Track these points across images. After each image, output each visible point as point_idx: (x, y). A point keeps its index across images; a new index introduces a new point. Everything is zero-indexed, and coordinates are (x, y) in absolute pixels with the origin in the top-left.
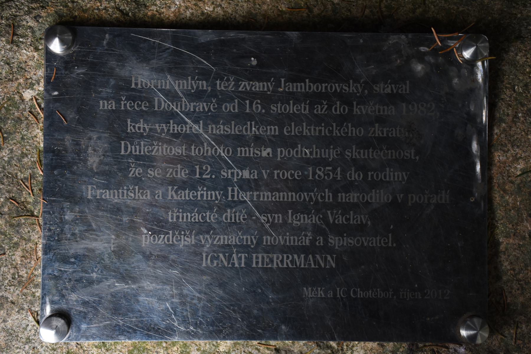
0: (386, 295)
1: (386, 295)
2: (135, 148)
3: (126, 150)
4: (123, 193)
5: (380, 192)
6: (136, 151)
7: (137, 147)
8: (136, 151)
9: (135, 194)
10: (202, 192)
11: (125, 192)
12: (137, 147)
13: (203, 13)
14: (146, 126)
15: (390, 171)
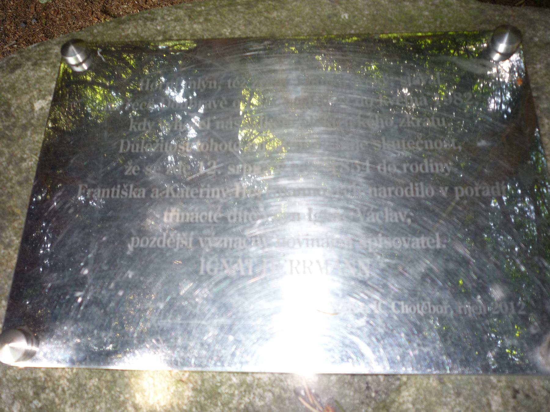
0: (469, 192)
1: (469, 192)
2: (135, 146)
3: (125, 147)
4: (116, 191)
5: (419, 186)
6: (135, 149)
7: (138, 145)
8: (135, 149)
9: (128, 193)
10: (205, 189)
11: (118, 191)
12: (138, 145)
13: (220, 34)
14: (149, 124)
15: (429, 163)
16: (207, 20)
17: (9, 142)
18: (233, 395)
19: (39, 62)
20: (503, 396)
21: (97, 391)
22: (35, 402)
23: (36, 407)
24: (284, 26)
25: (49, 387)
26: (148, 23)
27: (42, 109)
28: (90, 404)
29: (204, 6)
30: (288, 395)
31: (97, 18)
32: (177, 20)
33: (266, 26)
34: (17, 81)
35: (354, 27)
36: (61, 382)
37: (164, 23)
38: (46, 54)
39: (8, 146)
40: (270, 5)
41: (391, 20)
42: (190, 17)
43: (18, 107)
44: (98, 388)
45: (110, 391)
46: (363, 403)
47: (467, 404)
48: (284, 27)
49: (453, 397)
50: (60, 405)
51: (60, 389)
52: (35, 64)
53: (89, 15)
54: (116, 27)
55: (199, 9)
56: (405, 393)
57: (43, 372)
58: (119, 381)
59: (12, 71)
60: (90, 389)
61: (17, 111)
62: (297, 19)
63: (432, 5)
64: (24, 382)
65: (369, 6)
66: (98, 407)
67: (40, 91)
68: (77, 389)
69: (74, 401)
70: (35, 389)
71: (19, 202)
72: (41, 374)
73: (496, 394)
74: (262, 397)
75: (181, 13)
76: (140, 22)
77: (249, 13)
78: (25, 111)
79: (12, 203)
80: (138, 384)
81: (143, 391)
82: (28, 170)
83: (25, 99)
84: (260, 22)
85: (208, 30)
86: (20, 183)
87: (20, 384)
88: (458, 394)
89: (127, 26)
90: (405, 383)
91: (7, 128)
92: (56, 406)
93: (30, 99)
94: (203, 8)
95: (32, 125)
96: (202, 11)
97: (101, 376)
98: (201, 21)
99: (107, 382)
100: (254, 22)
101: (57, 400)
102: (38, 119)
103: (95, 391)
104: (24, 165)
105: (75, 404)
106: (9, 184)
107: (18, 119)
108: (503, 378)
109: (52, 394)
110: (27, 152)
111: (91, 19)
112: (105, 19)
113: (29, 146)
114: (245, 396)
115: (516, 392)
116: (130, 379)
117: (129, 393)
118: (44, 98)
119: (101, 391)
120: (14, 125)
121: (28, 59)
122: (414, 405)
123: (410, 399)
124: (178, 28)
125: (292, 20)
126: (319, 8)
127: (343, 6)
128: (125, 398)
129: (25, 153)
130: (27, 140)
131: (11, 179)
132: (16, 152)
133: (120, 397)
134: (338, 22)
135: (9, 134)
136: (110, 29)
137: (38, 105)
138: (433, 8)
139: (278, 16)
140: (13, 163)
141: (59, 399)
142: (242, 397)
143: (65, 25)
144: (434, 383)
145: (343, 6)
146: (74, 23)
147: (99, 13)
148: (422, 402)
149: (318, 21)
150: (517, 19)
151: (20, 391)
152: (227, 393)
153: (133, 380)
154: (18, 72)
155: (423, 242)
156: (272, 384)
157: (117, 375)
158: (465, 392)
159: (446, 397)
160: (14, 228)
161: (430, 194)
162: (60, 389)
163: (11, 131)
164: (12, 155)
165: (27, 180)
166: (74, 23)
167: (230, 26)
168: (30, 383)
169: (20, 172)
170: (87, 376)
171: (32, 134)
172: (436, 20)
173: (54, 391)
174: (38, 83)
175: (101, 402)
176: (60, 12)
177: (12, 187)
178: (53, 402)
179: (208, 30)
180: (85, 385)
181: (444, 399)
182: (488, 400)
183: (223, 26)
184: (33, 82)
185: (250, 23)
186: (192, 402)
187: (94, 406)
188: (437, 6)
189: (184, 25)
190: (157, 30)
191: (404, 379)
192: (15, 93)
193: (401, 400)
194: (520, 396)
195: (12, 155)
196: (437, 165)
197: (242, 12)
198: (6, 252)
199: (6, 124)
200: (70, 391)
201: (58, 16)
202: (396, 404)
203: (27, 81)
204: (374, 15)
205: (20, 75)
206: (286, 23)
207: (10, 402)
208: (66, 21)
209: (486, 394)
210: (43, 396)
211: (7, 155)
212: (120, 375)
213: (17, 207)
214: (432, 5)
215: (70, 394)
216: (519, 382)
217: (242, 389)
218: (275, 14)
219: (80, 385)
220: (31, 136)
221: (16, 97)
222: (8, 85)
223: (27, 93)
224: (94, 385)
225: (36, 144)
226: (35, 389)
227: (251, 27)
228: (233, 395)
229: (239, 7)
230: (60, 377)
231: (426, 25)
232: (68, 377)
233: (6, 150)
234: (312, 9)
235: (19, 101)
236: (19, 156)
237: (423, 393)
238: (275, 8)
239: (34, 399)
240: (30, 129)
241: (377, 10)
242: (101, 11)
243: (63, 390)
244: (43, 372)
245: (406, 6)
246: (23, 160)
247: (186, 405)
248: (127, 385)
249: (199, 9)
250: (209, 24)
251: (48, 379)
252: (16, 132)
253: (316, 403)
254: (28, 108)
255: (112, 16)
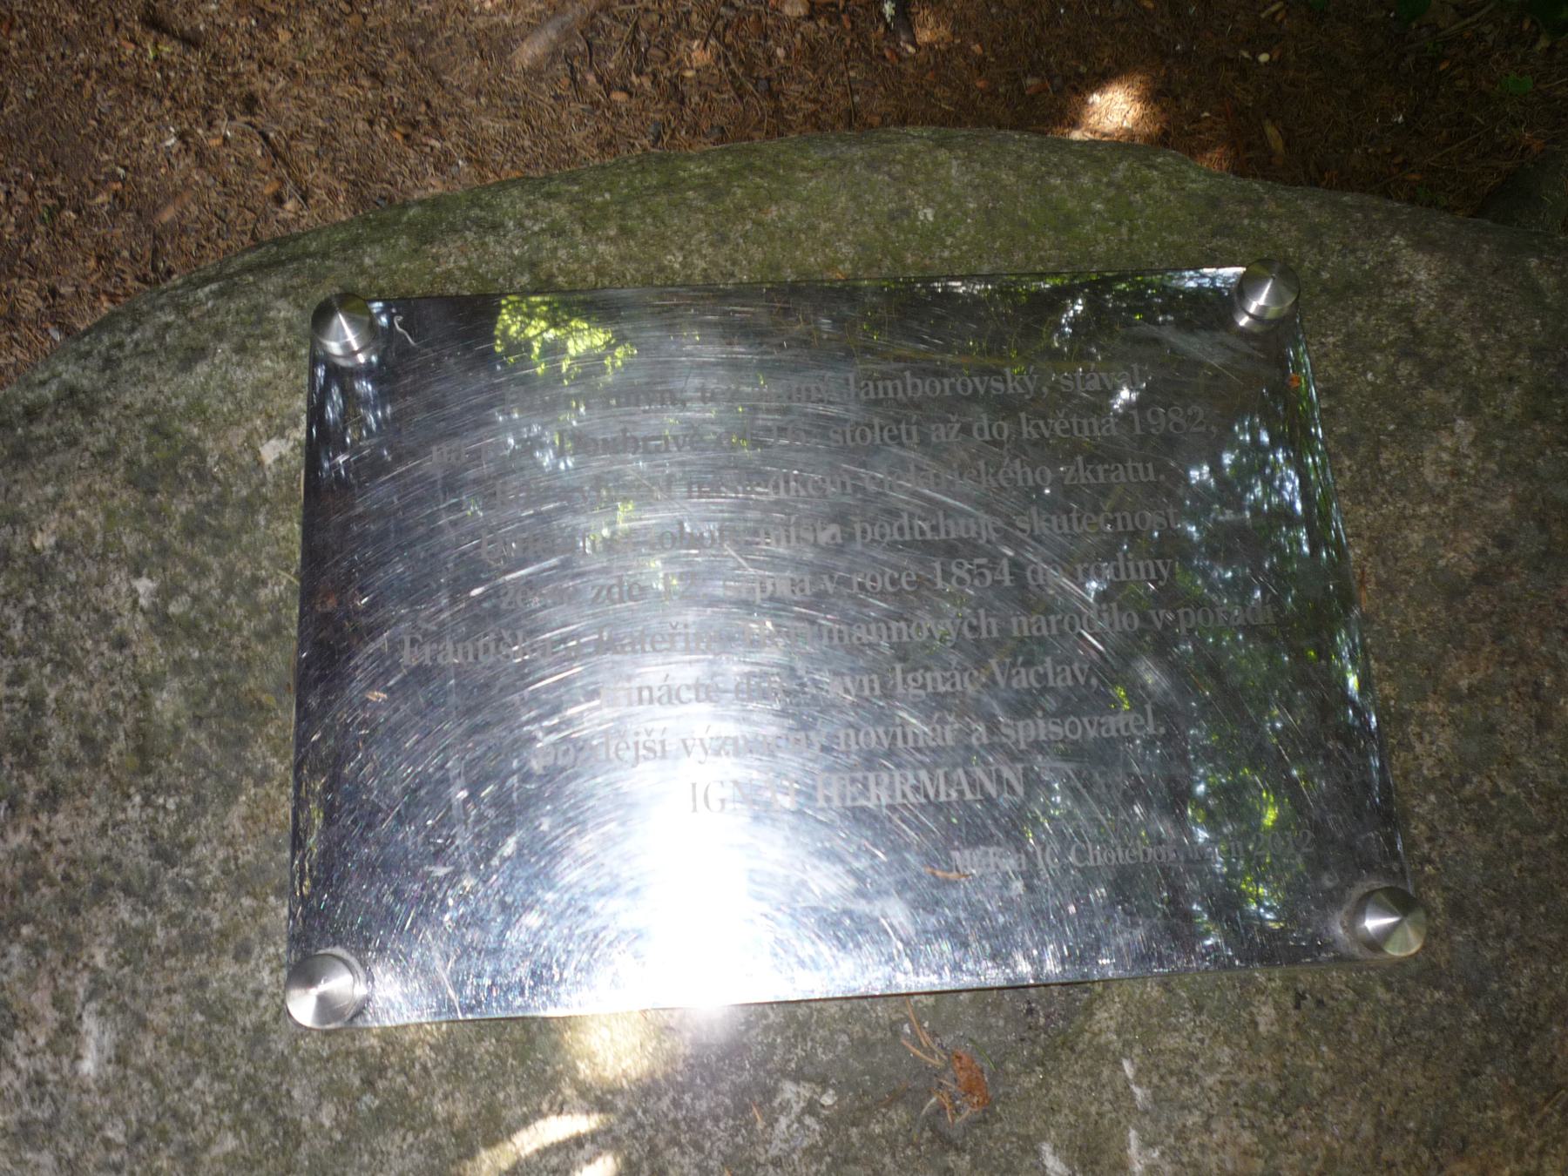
16: (625, 231)
17: (217, 541)
18: (772, 1046)
19: (250, 343)
20: (1277, 1006)
21: (496, 1062)
22: (367, 1098)
23: (370, 1109)
24: (798, 245)
25: (392, 1066)
26: (490, 239)
27: (280, 460)
28: (484, 1090)
29: (610, 191)
30: (880, 1035)
31: (132, 40)
32: (557, 231)
33: (760, 244)
34: (204, 391)
35: (949, 241)
36: (418, 1052)
37: (526, 240)
38: (260, 322)
39: (217, 551)
40: (758, 187)
41: (1026, 225)
42: (582, 221)
43: (223, 457)
44: (498, 1056)
45: (523, 1063)
46: (1022, 1040)
47: (1215, 1025)
48: (798, 245)
49: (1190, 1015)
50: (420, 1098)
51: (418, 1066)
52: (241, 349)
53: (109, 32)
54: (416, 251)
55: (599, 199)
56: (1101, 1015)
57: (377, 1036)
58: (541, 1040)
59: (187, 365)
60: (481, 1060)
61: (223, 466)
62: (825, 226)
63: (1109, 184)
64: (339, 1059)
65: (976, 188)
66: (501, 1096)
67: (270, 417)
68: (455, 1063)
69: (448, 1087)
70: (363, 1073)
71: (269, 680)
72: (374, 1042)
73: (1265, 1004)
74: (829, 1044)
75: (560, 211)
76: (470, 235)
77: (718, 213)
78: (240, 466)
79: (252, 683)
80: (579, 1041)
81: (591, 1057)
82: (276, 605)
83: (237, 437)
84: (745, 236)
85: (632, 258)
86: (262, 637)
87: (330, 1065)
88: (1199, 1009)
89: (443, 250)
90: (1101, 996)
91: (207, 508)
92: (411, 1103)
93: (248, 438)
94: (607, 196)
95: (266, 500)
96: (606, 204)
97: (501, 1034)
98: (612, 233)
99: (514, 1043)
100: (732, 235)
101: (412, 1090)
102: (277, 485)
103: (492, 1063)
104: (264, 594)
105: (452, 1094)
106: (236, 641)
107: (226, 485)
108: (1277, 973)
109: (400, 1079)
110: (265, 563)
111: (114, 43)
112: (156, 44)
113: (268, 548)
114: (796, 1047)
115: (1299, 997)
116: (561, 1034)
117: (564, 1061)
118: (281, 433)
119: (504, 1063)
120: (222, 500)
121: (219, 334)
122: (1119, 1035)
123: (1112, 1024)
124: (562, 253)
125: (813, 228)
126: (869, 197)
127: (921, 190)
128: (557, 1073)
129: (260, 567)
130: (259, 535)
131: (239, 628)
132: (240, 565)
133: (544, 1071)
134: (913, 230)
135: (213, 523)
136: (403, 257)
137: (270, 451)
138: (1112, 192)
139: (782, 218)
140: (238, 590)
141: (417, 1088)
142: (790, 1047)
143: (38, 62)
144: (1154, 991)
145: (921, 190)
146: (63, 56)
147: (138, 28)
148: (1134, 1028)
149: (870, 229)
150: (1285, 225)
151: (331, 1079)
152: (761, 1043)
153: (568, 1035)
154: (202, 368)
155: (1122, 726)
156: (847, 1018)
157: (534, 1027)
158: (1210, 1005)
159: (1177, 1016)
160: (269, 738)
161: (1131, 626)
162: (418, 1066)
163: (217, 515)
164: (230, 573)
165: (277, 628)
166: (63, 56)
167: (681, 248)
168: (352, 1060)
169: (256, 610)
170: (473, 1035)
171: (268, 522)
172: (1119, 223)
173: (403, 1071)
174: (260, 397)
175: (508, 1083)
176: (19, 21)
177: (245, 647)
178: (403, 1095)
179: (632, 258)
180: (470, 1053)
181: (1173, 1020)
182: (1251, 1014)
183: (665, 247)
184: (248, 394)
185: (724, 239)
186: (693, 1066)
187: (493, 1093)
188: (1119, 187)
189: (574, 246)
190: (512, 256)
191: (1099, 988)
192: (206, 422)
193: (1096, 1028)
194: (1309, 1002)
195: (230, 573)
196: (1141, 564)
197: (701, 210)
198: (261, 792)
199: (203, 498)
200: (439, 1069)
201: (14, 34)
202: (1087, 1036)
203: (233, 393)
204: (987, 212)
205: (209, 376)
206: (803, 237)
207: (313, 1103)
208: (41, 50)
209: (1248, 1004)
210: (380, 1084)
211: (219, 573)
212: (540, 1028)
213: (265, 691)
214: (1109, 184)
215: (441, 1076)
216: (1306, 978)
217: (790, 1033)
218: (774, 212)
219: (458, 1054)
220: (267, 527)
221: (214, 431)
222: (183, 401)
223: (238, 423)
224: (487, 1052)
225: (282, 544)
226: (363, 1073)
227: (726, 249)
228: (772, 1046)
229: (690, 194)
230: (413, 1044)
231: (1100, 236)
232: (433, 1041)
233: (214, 562)
234: (854, 198)
235: (222, 444)
236: (248, 573)
237: (1135, 1011)
238: (772, 198)
239: (364, 1092)
240: (263, 510)
241: (996, 199)
242: (142, 20)
243: (424, 1068)
244: (377, 1036)
245: (1056, 188)
246: (257, 582)
247: (681, 1073)
248: (556, 1047)
249: (599, 199)
250: (632, 243)
251: (390, 1049)
252: (230, 519)
253: (935, 1047)
254: (248, 458)
255: (175, 37)
